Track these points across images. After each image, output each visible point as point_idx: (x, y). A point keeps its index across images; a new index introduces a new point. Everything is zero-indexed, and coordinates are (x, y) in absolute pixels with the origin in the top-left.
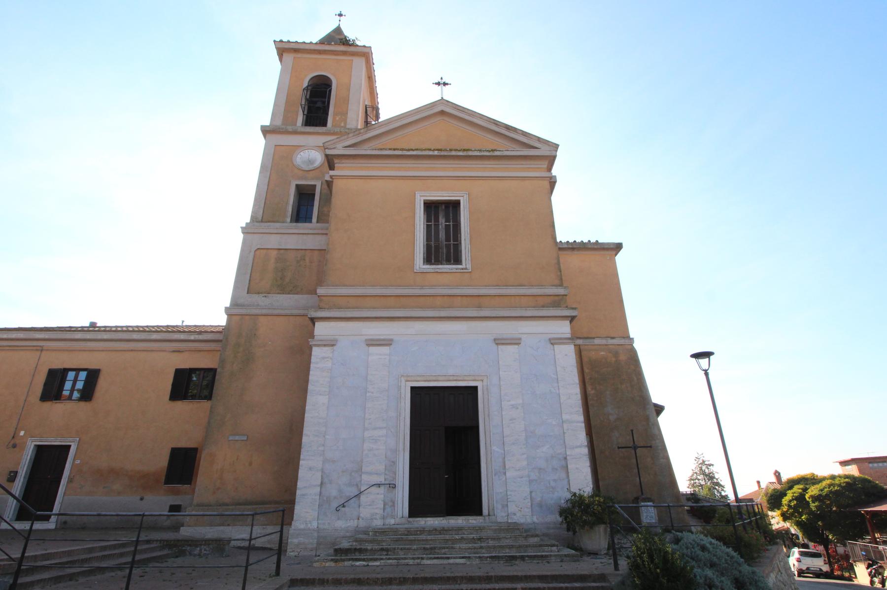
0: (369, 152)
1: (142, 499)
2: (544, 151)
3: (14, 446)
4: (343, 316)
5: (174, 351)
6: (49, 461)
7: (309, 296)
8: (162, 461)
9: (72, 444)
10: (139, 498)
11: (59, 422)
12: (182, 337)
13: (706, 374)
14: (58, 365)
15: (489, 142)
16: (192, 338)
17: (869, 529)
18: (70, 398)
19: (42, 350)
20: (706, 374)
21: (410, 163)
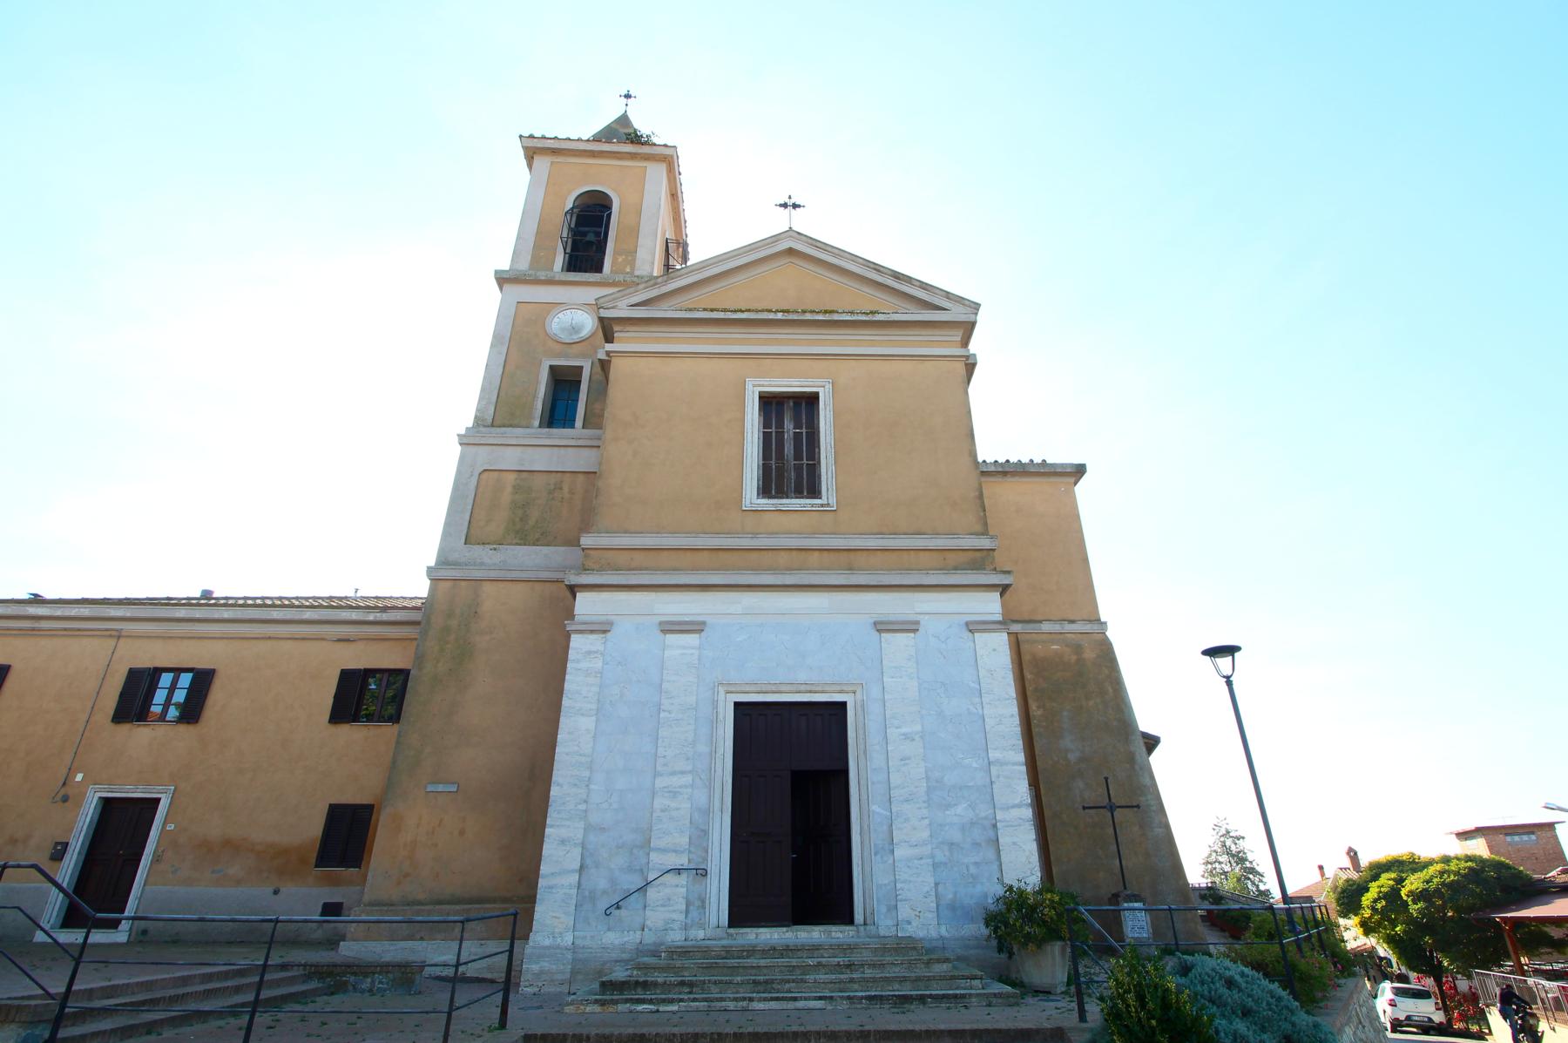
1: (276, 892)
2: (956, 314)
3: (65, 799)
6: (122, 825)
8: (313, 828)
10: (271, 890)
11: (143, 759)
13: (1229, 683)
20: (1229, 683)
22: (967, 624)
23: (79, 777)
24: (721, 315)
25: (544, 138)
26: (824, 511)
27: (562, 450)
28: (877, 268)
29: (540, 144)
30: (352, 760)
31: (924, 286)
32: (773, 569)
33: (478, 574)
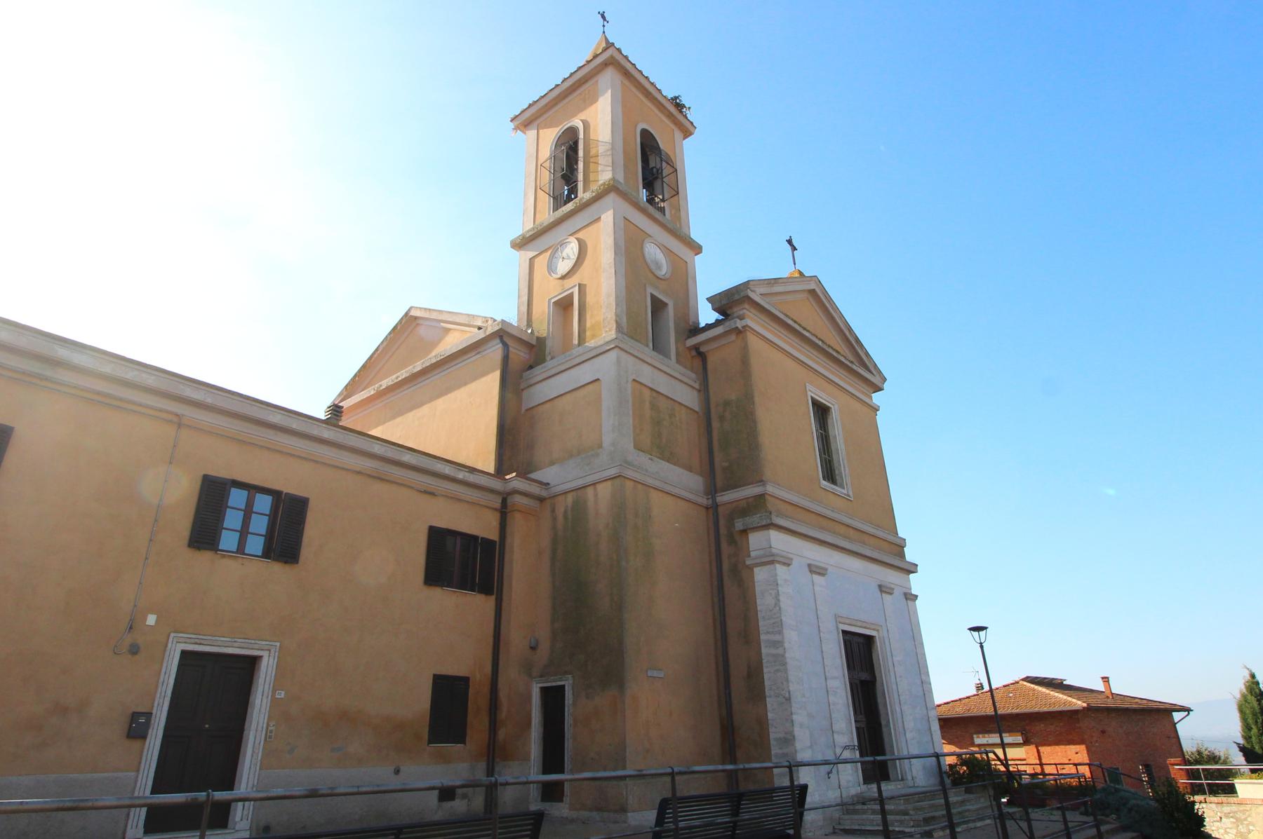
0: (766, 306)
1: (397, 772)
2: (875, 380)
3: (134, 650)
4: (307, 442)
5: (425, 492)
6: (214, 693)
7: (686, 472)
8: (421, 701)
9: (265, 654)
10: (392, 769)
11: (233, 601)
12: (447, 470)
13: (982, 647)
14: (222, 471)
15: (834, 341)
16: (461, 475)
17: (219, 795)
18: (241, 549)
19: (180, 425)
20: (982, 647)
21: (795, 341)
22: (809, 566)
23: (151, 620)
24: (790, 322)
25: (626, 57)
26: (846, 498)
27: (656, 371)
28: (850, 329)
29: (623, 62)
30: (451, 629)
31: (867, 354)
32: (846, 537)
33: (650, 481)
